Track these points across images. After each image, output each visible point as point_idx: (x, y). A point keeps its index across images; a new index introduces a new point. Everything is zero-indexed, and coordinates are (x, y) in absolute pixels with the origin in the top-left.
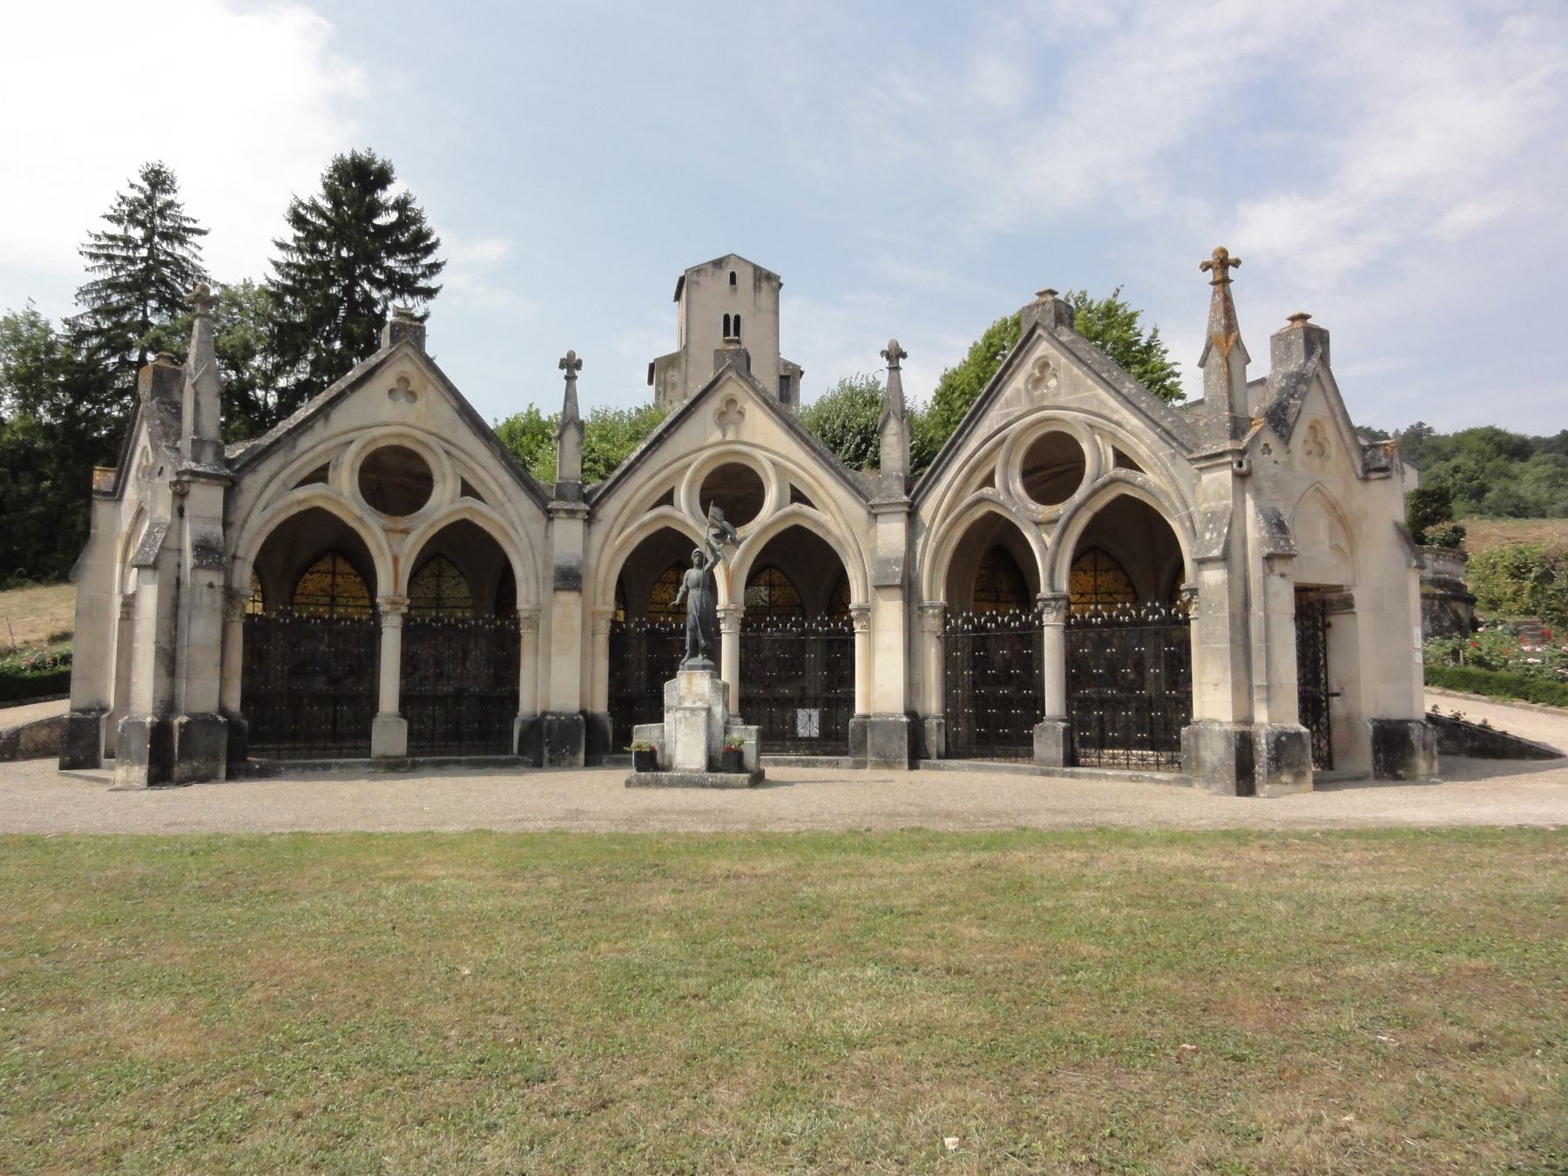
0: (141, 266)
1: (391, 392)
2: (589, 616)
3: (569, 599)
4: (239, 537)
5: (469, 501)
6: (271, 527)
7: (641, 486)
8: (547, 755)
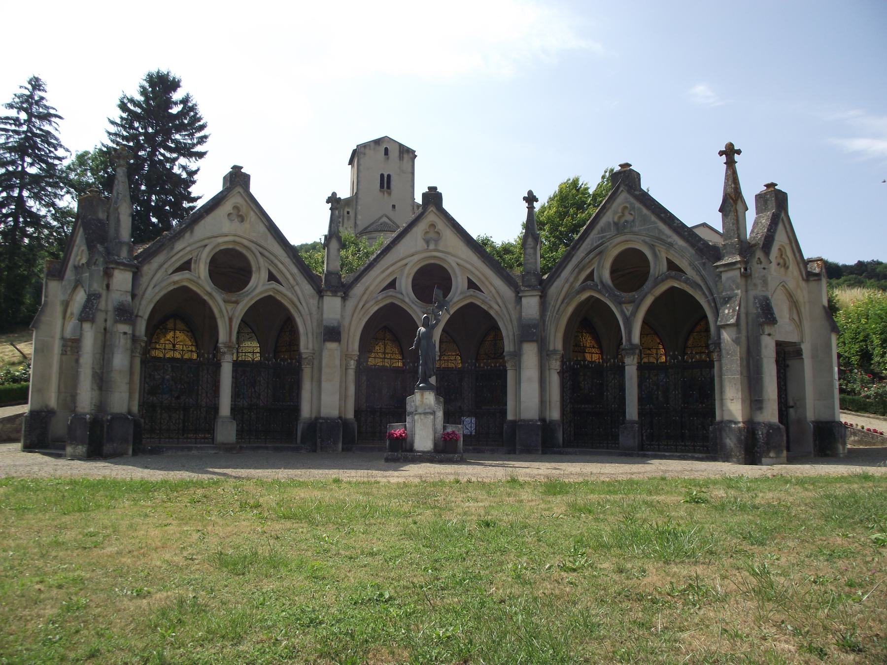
0: (23, 136)
1: (229, 215)
2: (346, 356)
3: (332, 346)
4: (140, 304)
5: (274, 285)
6: (158, 298)
7: (376, 279)
8: (319, 444)
